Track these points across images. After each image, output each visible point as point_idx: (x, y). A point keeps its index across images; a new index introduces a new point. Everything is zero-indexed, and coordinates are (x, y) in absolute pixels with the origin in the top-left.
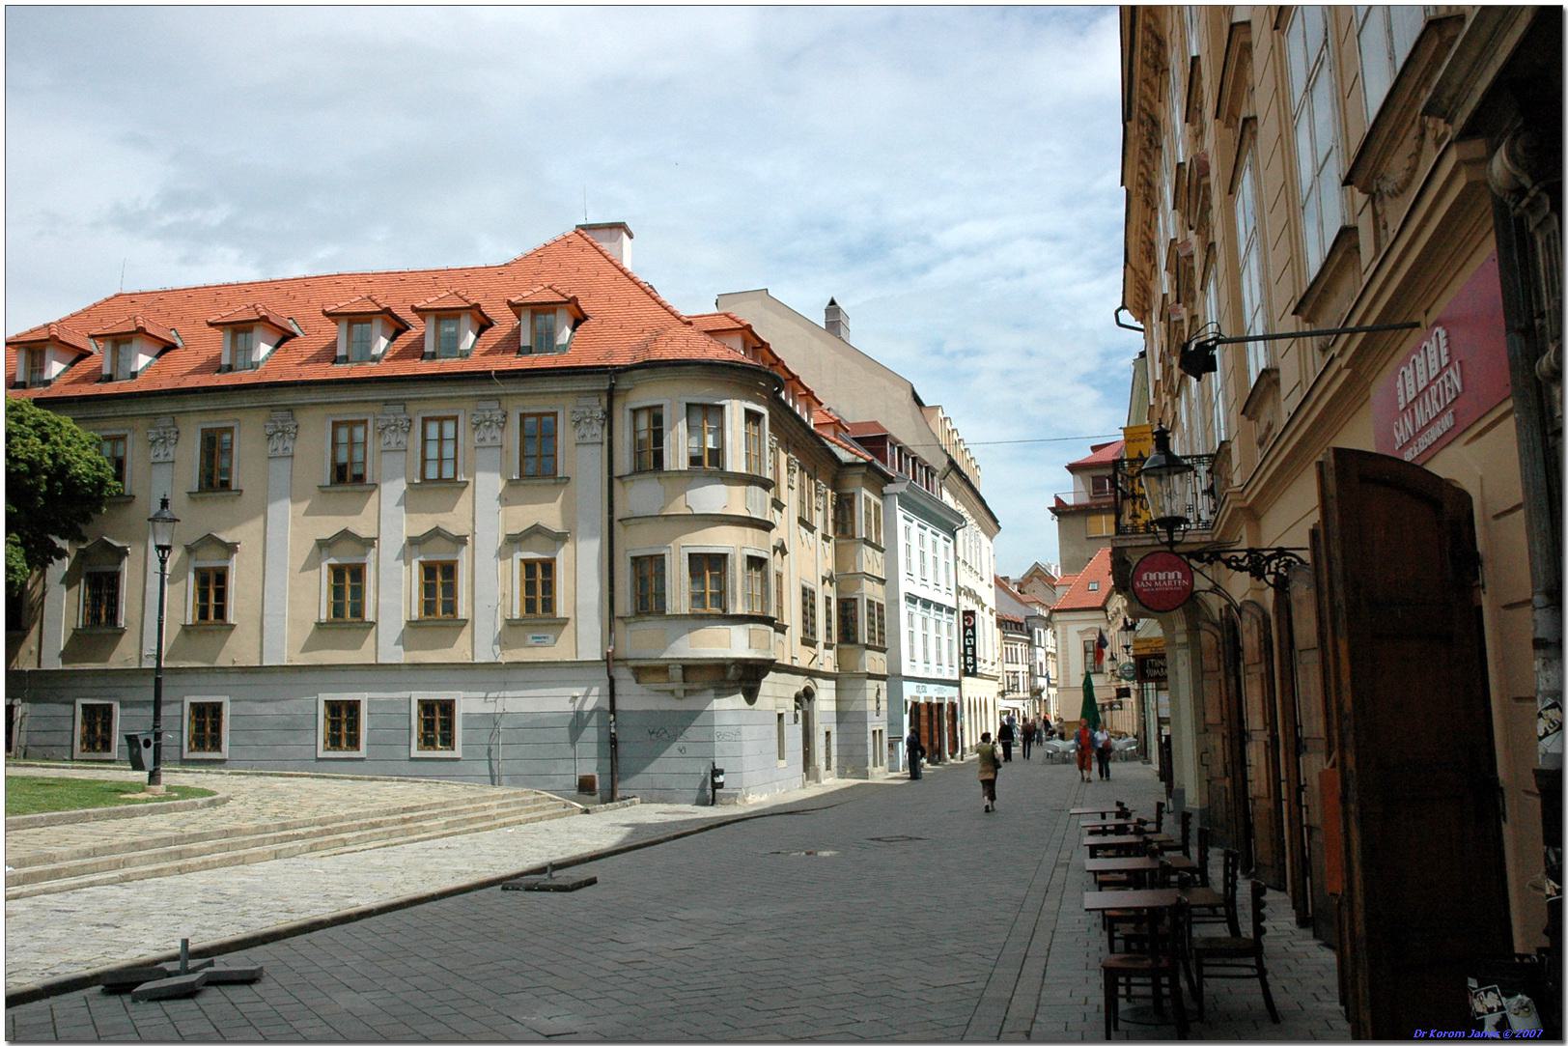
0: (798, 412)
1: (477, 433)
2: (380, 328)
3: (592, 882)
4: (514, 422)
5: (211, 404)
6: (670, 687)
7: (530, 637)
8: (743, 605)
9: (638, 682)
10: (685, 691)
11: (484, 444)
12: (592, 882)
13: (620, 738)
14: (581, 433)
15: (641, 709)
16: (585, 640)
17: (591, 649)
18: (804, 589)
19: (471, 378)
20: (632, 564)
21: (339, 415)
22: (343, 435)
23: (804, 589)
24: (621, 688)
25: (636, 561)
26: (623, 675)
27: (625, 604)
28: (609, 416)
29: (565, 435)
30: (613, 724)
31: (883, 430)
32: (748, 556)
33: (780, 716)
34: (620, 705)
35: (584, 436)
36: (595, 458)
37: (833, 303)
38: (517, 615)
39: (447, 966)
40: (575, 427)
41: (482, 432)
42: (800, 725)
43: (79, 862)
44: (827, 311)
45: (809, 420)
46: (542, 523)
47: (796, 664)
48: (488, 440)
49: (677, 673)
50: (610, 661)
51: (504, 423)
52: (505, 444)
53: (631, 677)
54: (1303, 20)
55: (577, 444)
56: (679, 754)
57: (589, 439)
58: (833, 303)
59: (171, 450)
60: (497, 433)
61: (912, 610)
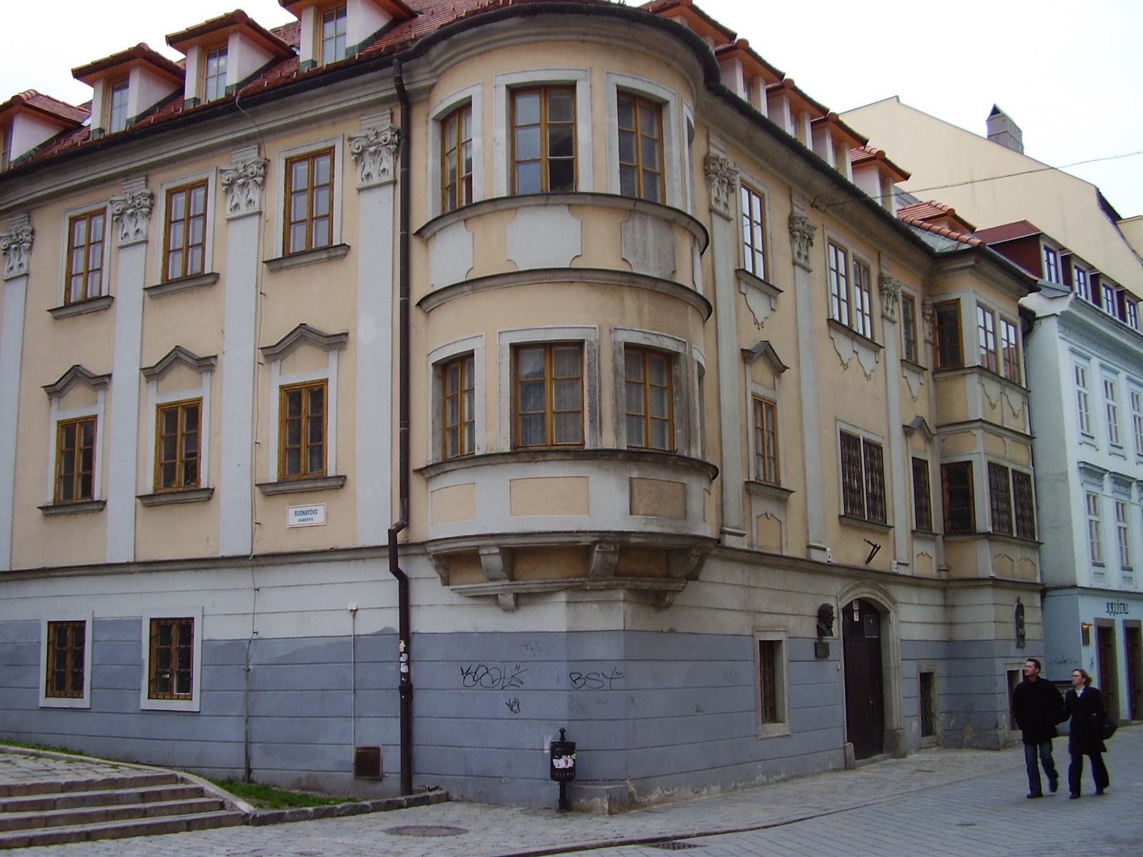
0: (809, 146)
1: (229, 198)
4: (278, 171)
6: (492, 587)
7: (291, 511)
8: (617, 432)
9: (446, 582)
10: (517, 596)
13: (417, 682)
15: (449, 629)
18: (848, 441)
20: (436, 376)
22: (82, 226)
23: (848, 441)
24: (419, 594)
26: (422, 571)
28: (403, 146)
29: (346, 177)
30: (404, 658)
31: (1035, 229)
32: (628, 346)
33: (769, 650)
34: (421, 622)
35: (368, 176)
36: (384, 205)
37: (995, 111)
38: (273, 476)
40: (356, 160)
41: (240, 197)
42: (835, 668)
44: (989, 120)
45: (886, 196)
46: (311, 323)
47: (816, 556)
48: (375, 175)
49: (493, 561)
51: (264, 177)
52: (263, 210)
53: (434, 573)
55: (360, 190)
56: (506, 712)
57: (375, 180)
58: (995, 111)
59: (142, 225)
60: (255, 194)
61: (1124, 498)
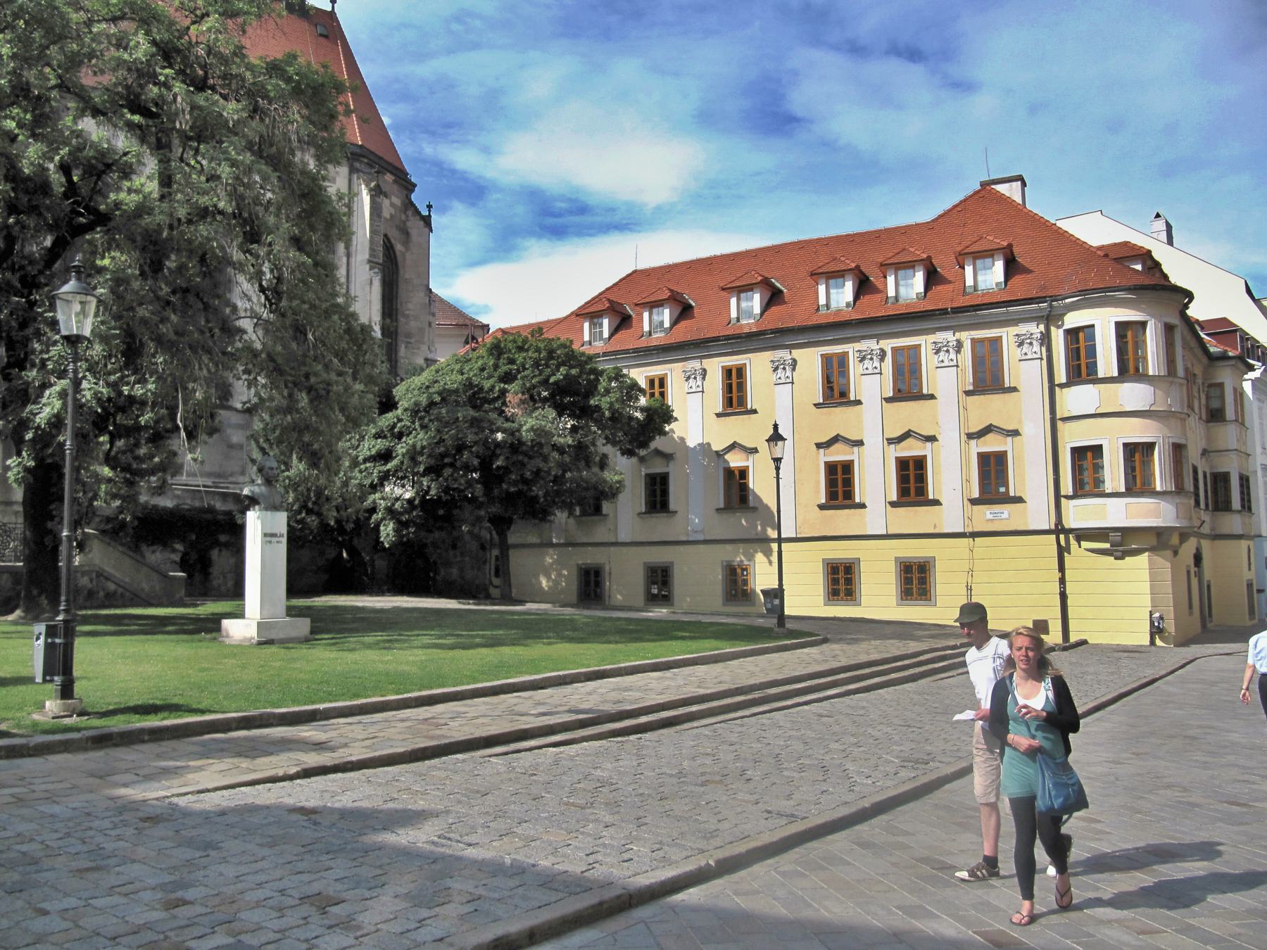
2: (410, 306)
3: (1250, 569)
4: (967, 346)
5: (644, 369)
11: (943, 365)
12: (1250, 569)
14: (1024, 351)
16: (1037, 513)
17: (1044, 520)
19: (878, 321)
21: (650, 371)
25: (1078, 453)
27: (1067, 486)
31: (1235, 326)
39: (719, 844)
43: (192, 763)
48: (1029, 353)
50: (1059, 529)
52: (960, 364)
54: (727, 867)
57: (946, 363)
